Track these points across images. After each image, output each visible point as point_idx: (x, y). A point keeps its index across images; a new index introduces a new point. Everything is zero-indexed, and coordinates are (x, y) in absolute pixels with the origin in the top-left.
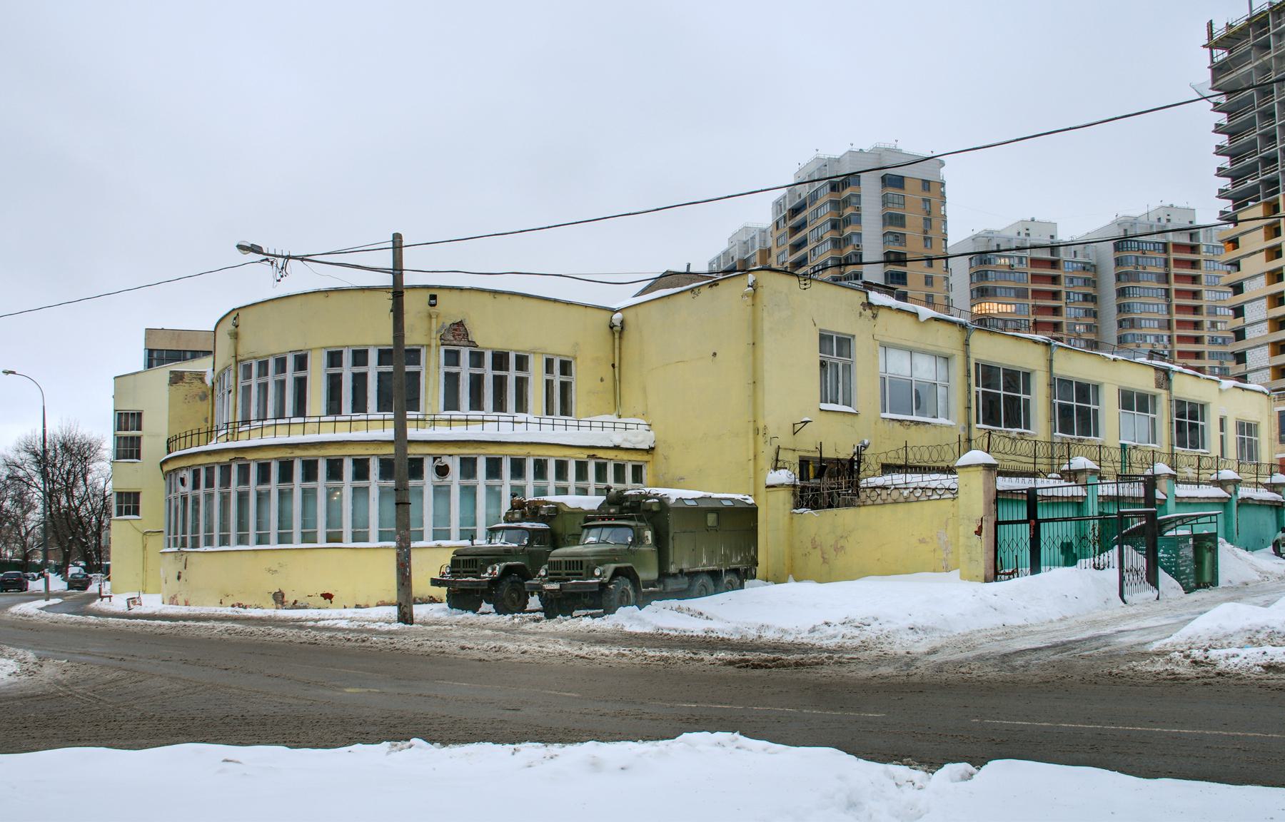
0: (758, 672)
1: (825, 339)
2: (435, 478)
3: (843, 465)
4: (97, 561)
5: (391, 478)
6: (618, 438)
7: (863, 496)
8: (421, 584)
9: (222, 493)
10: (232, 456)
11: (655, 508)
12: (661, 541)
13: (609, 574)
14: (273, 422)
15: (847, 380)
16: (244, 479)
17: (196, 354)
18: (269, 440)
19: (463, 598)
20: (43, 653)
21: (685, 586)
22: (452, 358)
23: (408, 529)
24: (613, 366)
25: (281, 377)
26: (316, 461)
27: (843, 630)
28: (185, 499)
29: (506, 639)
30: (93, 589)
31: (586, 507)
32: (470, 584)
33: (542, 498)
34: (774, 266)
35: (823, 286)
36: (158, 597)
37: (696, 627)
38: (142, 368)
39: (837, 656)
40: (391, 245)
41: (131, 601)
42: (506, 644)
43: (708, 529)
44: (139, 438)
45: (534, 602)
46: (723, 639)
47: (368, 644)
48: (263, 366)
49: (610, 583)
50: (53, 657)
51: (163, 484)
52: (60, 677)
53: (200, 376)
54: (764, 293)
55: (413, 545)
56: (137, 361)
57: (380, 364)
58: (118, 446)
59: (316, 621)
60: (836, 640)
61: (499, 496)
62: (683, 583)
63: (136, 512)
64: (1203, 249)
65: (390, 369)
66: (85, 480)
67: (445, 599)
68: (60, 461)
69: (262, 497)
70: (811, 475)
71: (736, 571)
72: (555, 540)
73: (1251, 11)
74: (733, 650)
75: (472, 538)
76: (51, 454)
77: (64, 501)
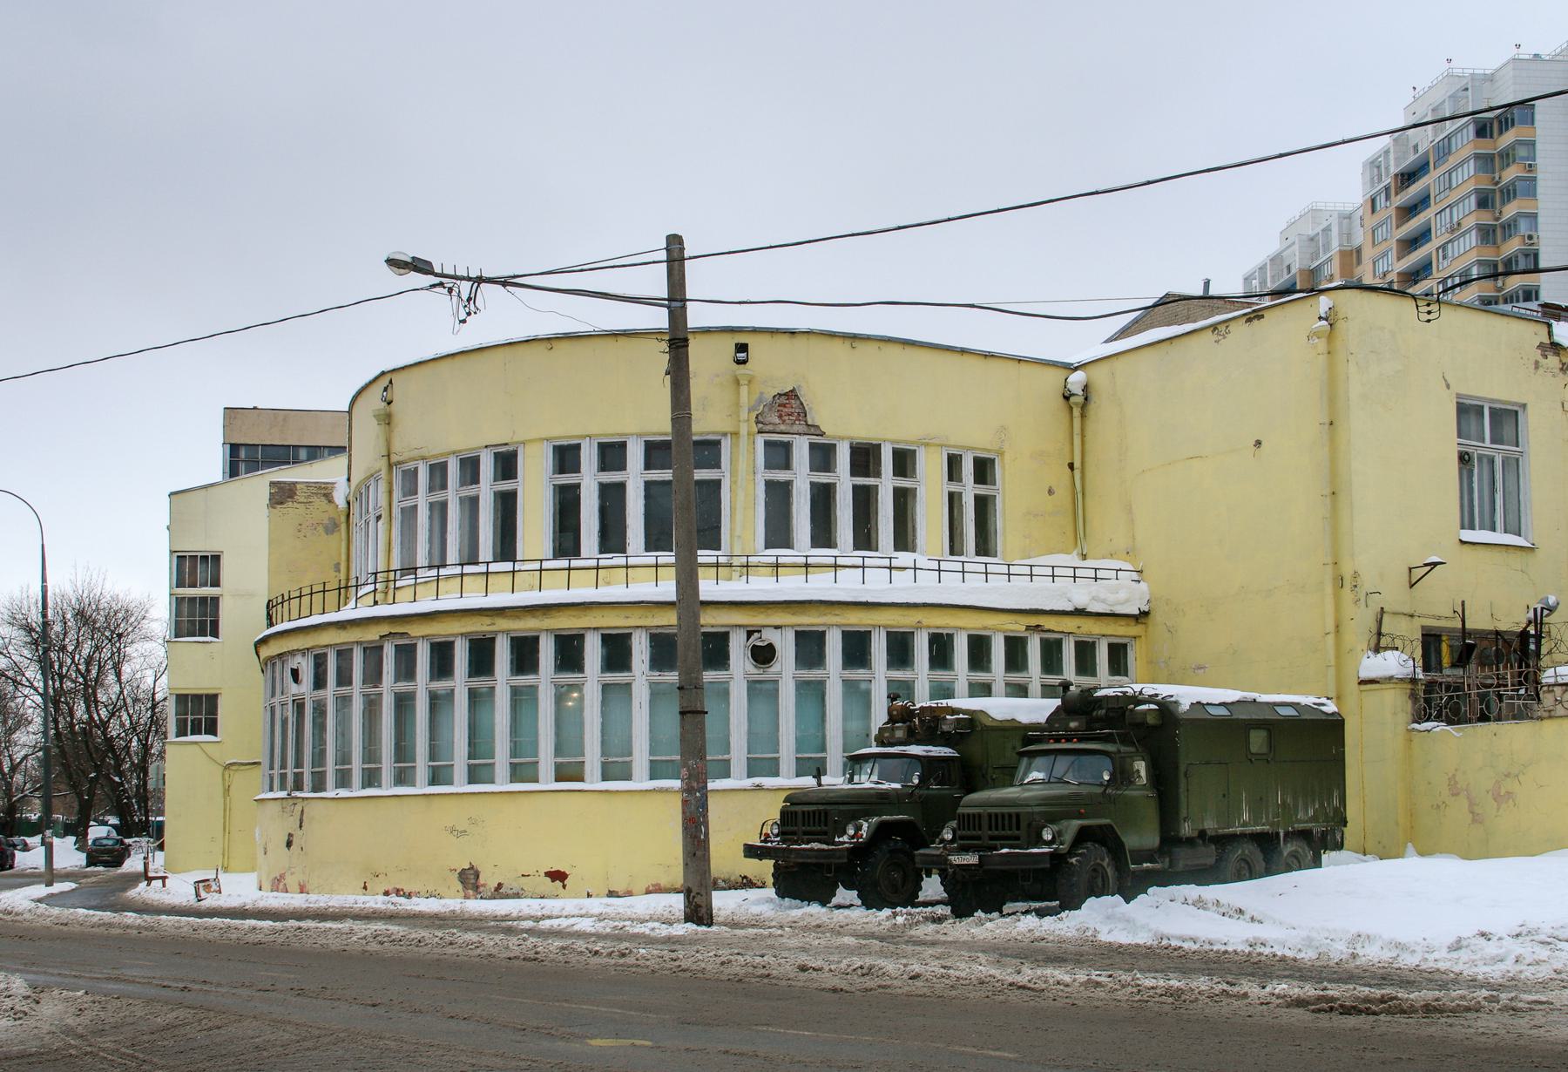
0: (1352, 1021)
1: (1467, 411)
2: (750, 666)
3: (1508, 643)
4: (140, 817)
5: (671, 668)
6: (1081, 595)
7: (1547, 700)
8: (725, 854)
9: (377, 695)
10: (385, 629)
11: (1151, 720)
12: (1164, 782)
13: (1068, 837)
14: (458, 570)
15: (1512, 487)
16: (406, 669)
17: (315, 453)
18: (449, 602)
19: (802, 878)
20: (41, 979)
21: (1211, 861)
22: (779, 455)
23: (703, 758)
24: (1071, 466)
25: (470, 491)
26: (536, 639)
27: (1516, 948)
28: (299, 706)
29: (881, 954)
30: (133, 864)
31: (1024, 719)
32: (816, 852)
33: (944, 703)
34: (1368, 281)
35: (1462, 315)
36: (251, 879)
37: (1232, 936)
38: (218, 477)
39: (1505, 995)
40: (663, 255)
41: (203, 885)
42: (881, 962)
43: (1251, 758)
44: (215, 600)
45: (932, 887)
46: (1283, 959)
47: (630, 960)
48: (438, 472)
49: (1070, 853)
50: (59, 985)
51: (258, 680)
52: (70, 1021)
53: (325, 491)
54: (1349, 331)
55: (711, 785)
56: (212, 466)
57: (648, 466)
58: (178, 613)
59: (537, 919)
60: (1502, 967)
61: (866, 697)
62: (1207, 855)
63: (212, 729)
65: (666, 475)
66: (119, 675)
67: (770, 880)
68: (75, 642)
69: (438, 702)
70: (1446, 661)
71: (1305, 835)
72: (968, 774)
74: (1303, 978)
75: (819, 773)
76: (58, 628)
77: (80, 711)
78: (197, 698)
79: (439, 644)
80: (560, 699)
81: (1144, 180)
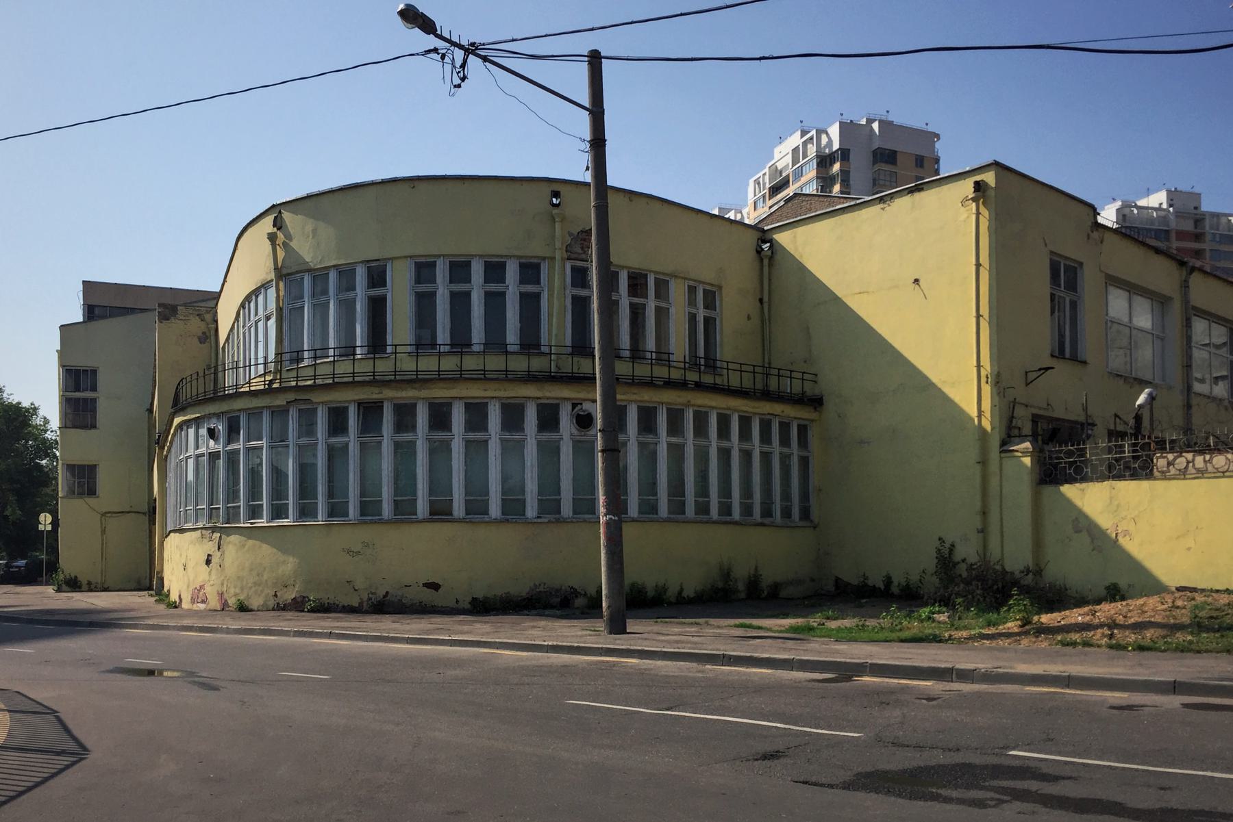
10: (291, 396)
24: (761, 301)
64: (1208, 237)
73: (144, 514)
78: (81, 467)
79: (334, 408)
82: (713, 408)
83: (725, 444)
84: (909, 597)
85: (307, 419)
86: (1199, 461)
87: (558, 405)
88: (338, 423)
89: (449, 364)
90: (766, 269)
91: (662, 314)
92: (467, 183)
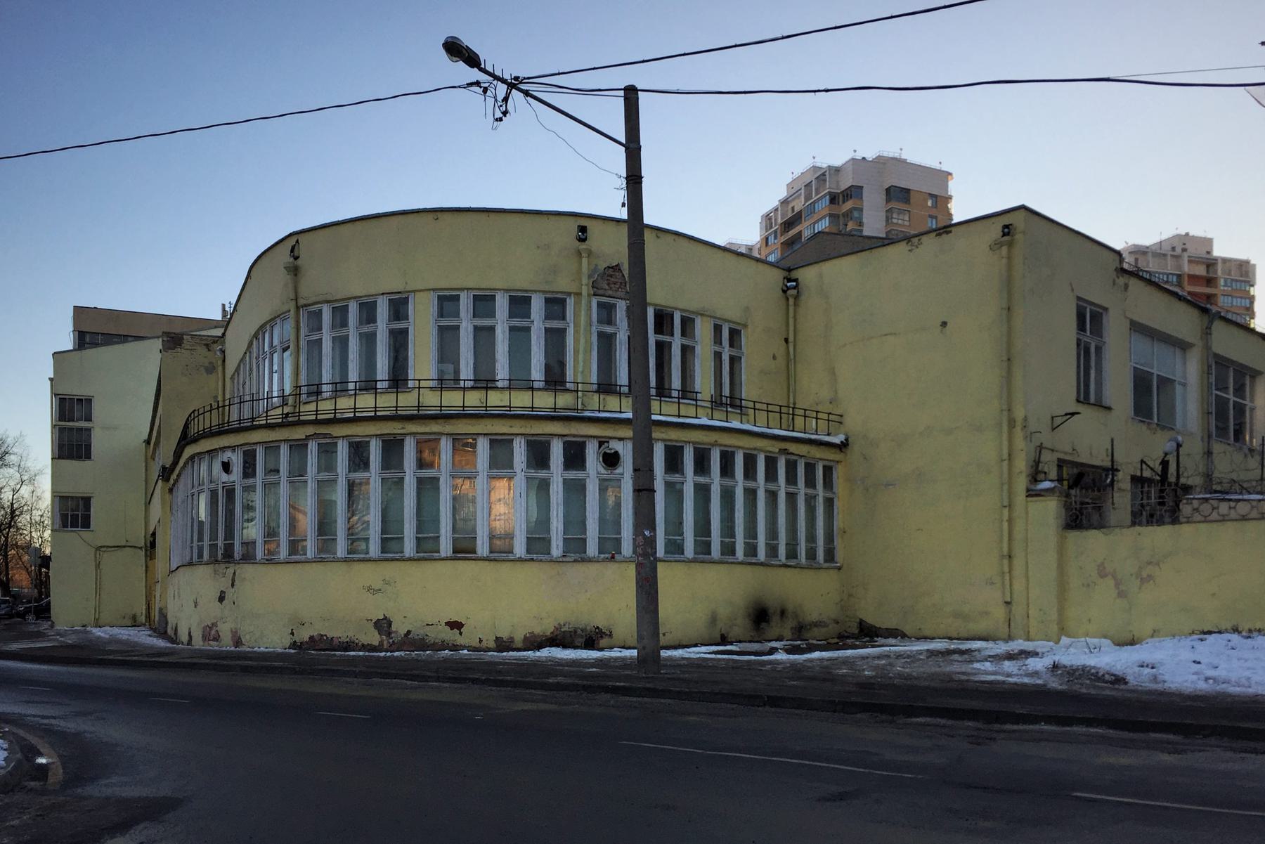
24: (786, 340)
58: (60, 438)
63: (86, 524)
80: (603, 490)
81: (779, 35)
82: (761, 450)
83: (751, 484)
84: (425, 679)
85: (328, 451)
86: (1224, 507)
87: (584, 443)
88: (359, 457)
89: (474, 399)
90: (791, 309)
91: (687, 351)
92: (492, 215)
